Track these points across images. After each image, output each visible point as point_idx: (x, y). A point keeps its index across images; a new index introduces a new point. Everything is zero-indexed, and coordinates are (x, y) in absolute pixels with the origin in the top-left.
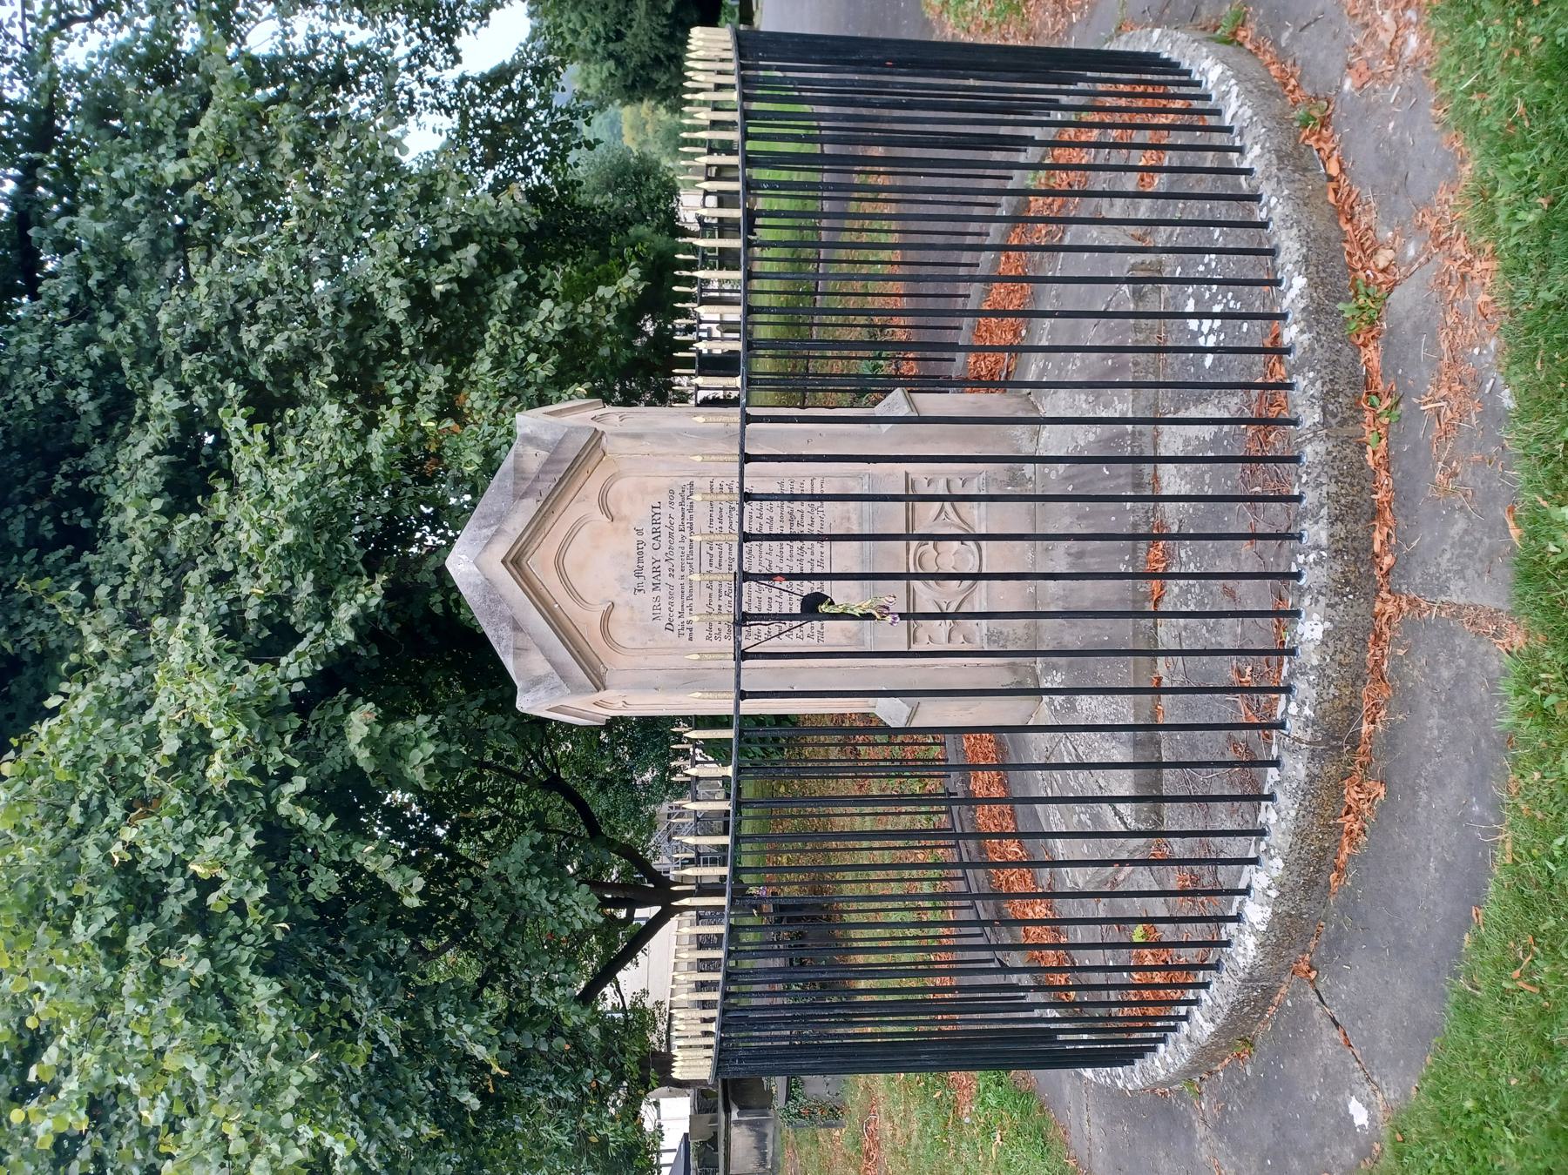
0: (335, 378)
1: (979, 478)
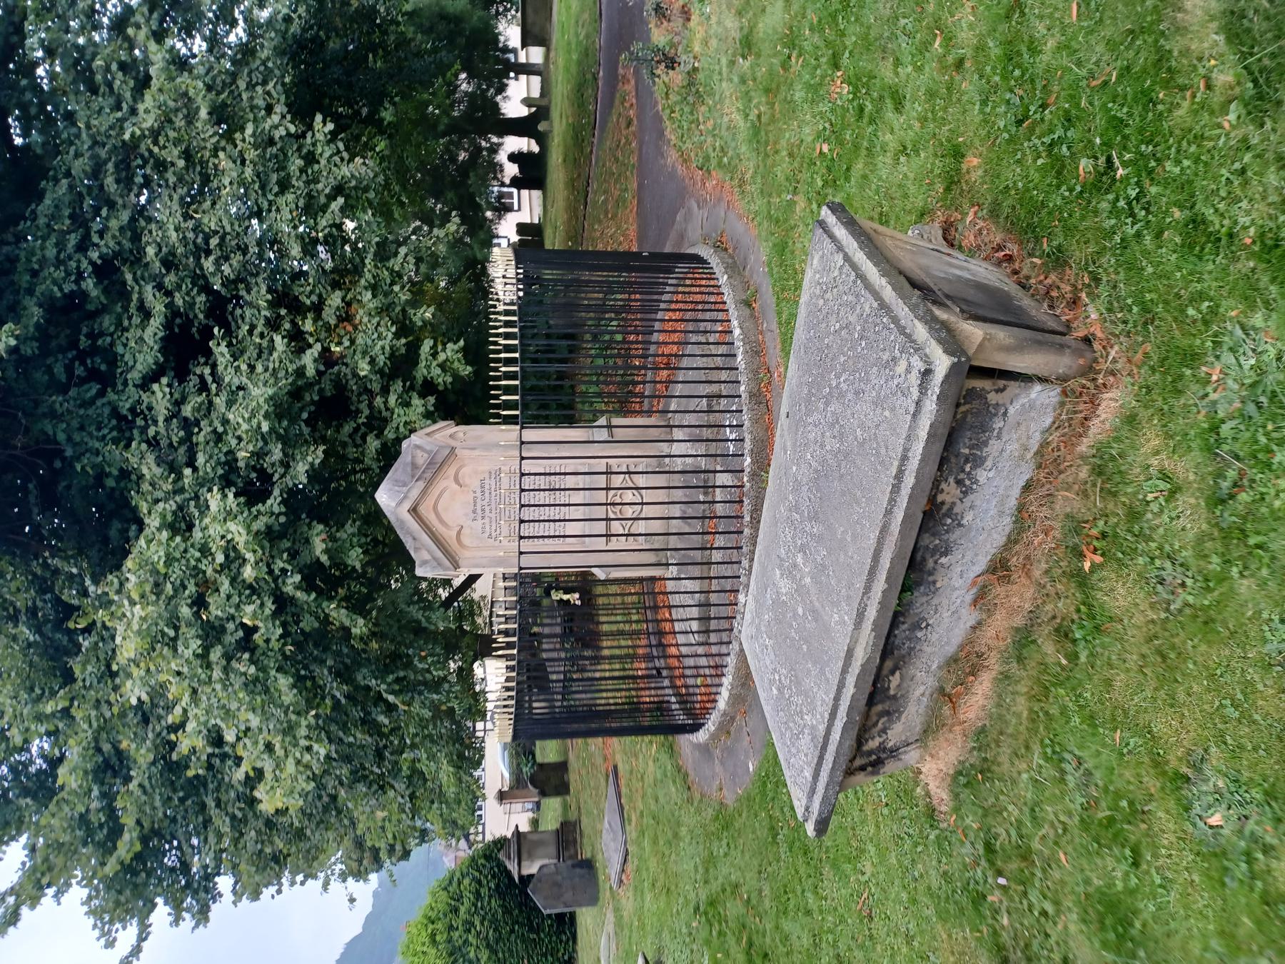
0: (269, 297)
1: (642, 465)
